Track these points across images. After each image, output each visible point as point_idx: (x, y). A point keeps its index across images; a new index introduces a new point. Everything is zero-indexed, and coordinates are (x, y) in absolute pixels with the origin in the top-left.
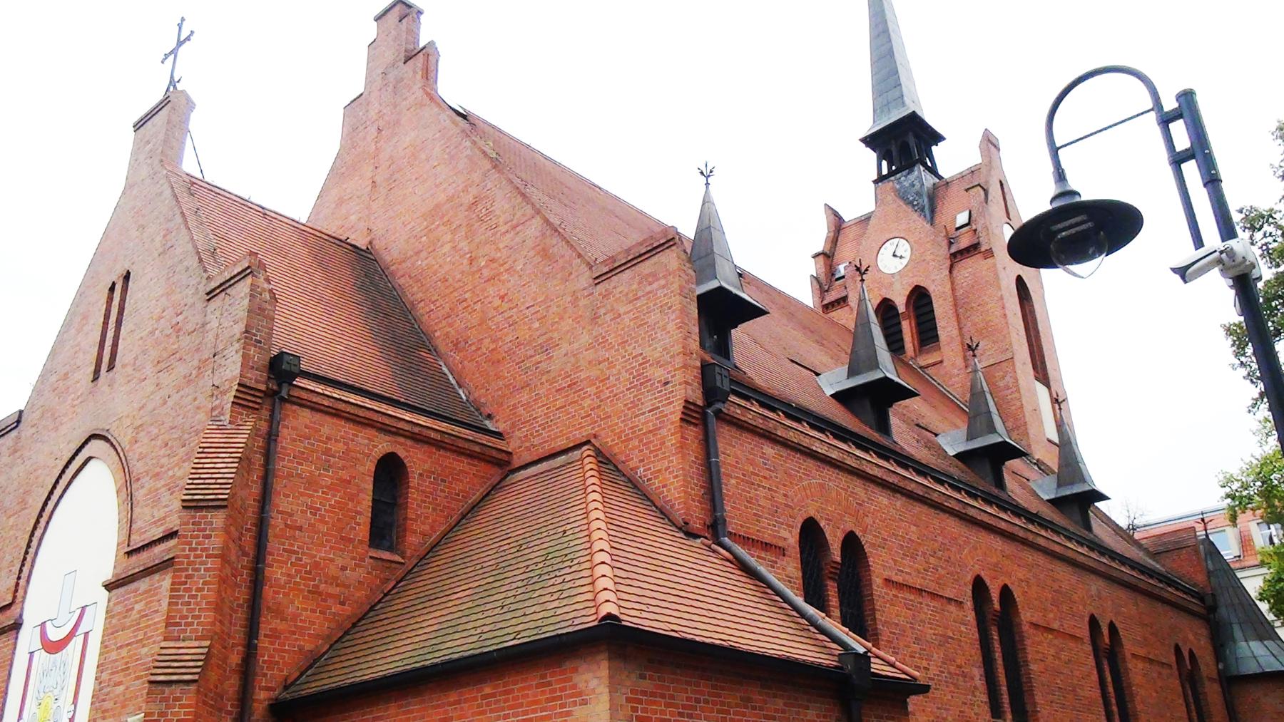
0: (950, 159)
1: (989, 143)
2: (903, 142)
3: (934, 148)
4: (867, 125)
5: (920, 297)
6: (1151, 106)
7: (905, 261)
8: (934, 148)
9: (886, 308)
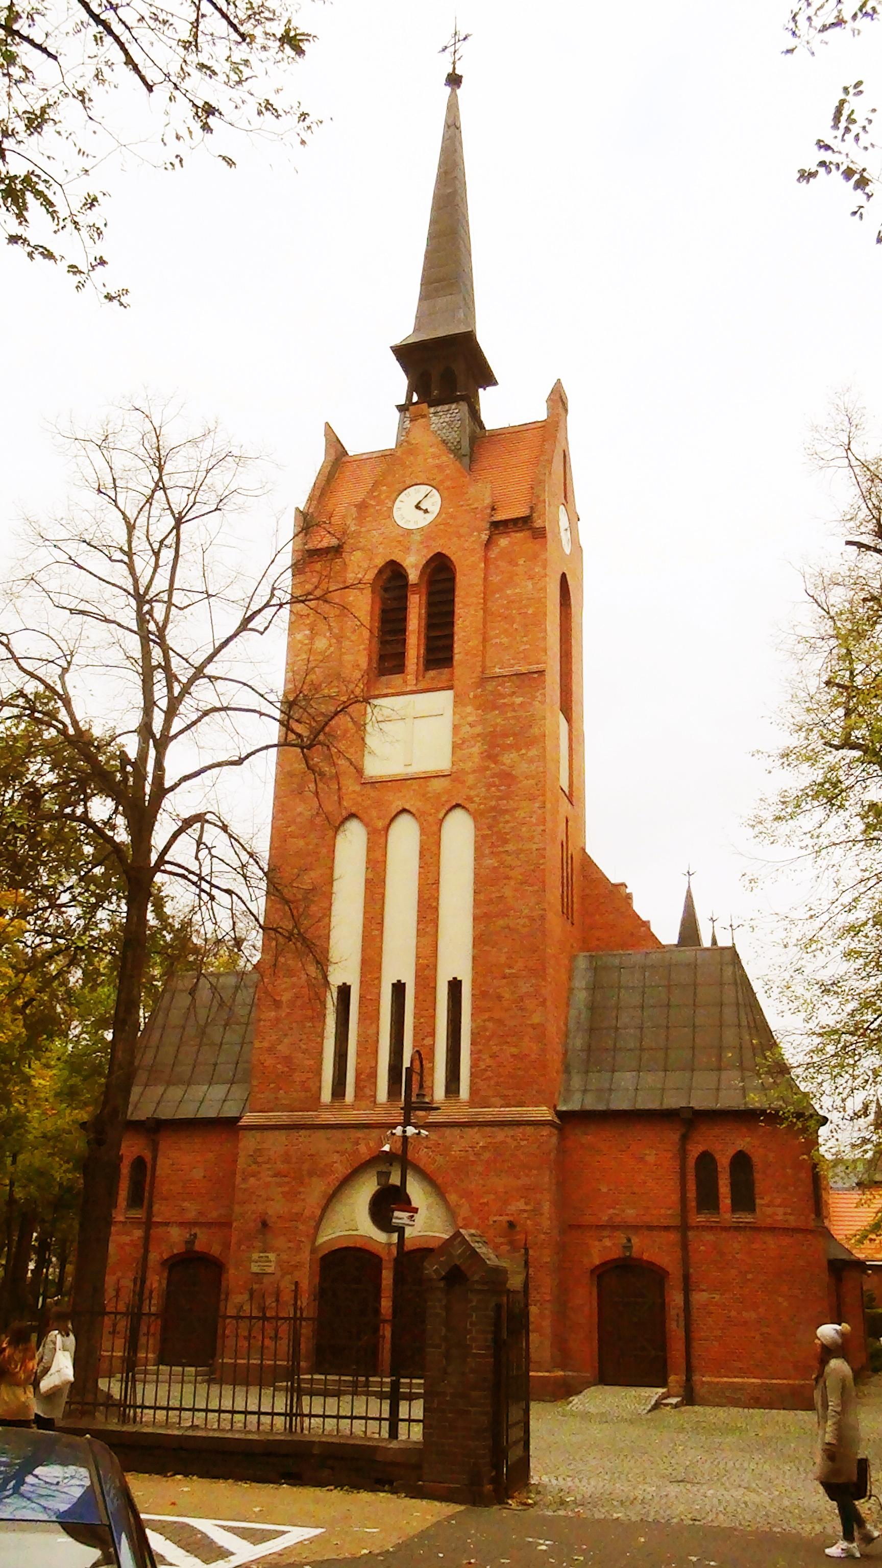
0: (498, 408)
1: (558, 400)
2: (444, 367)
3: (481, 390)
4: (404, 330)
5: (441, 570)
6: (175, 592)
7: (430, 518)
8: (481, 390)
9: (392, 577)
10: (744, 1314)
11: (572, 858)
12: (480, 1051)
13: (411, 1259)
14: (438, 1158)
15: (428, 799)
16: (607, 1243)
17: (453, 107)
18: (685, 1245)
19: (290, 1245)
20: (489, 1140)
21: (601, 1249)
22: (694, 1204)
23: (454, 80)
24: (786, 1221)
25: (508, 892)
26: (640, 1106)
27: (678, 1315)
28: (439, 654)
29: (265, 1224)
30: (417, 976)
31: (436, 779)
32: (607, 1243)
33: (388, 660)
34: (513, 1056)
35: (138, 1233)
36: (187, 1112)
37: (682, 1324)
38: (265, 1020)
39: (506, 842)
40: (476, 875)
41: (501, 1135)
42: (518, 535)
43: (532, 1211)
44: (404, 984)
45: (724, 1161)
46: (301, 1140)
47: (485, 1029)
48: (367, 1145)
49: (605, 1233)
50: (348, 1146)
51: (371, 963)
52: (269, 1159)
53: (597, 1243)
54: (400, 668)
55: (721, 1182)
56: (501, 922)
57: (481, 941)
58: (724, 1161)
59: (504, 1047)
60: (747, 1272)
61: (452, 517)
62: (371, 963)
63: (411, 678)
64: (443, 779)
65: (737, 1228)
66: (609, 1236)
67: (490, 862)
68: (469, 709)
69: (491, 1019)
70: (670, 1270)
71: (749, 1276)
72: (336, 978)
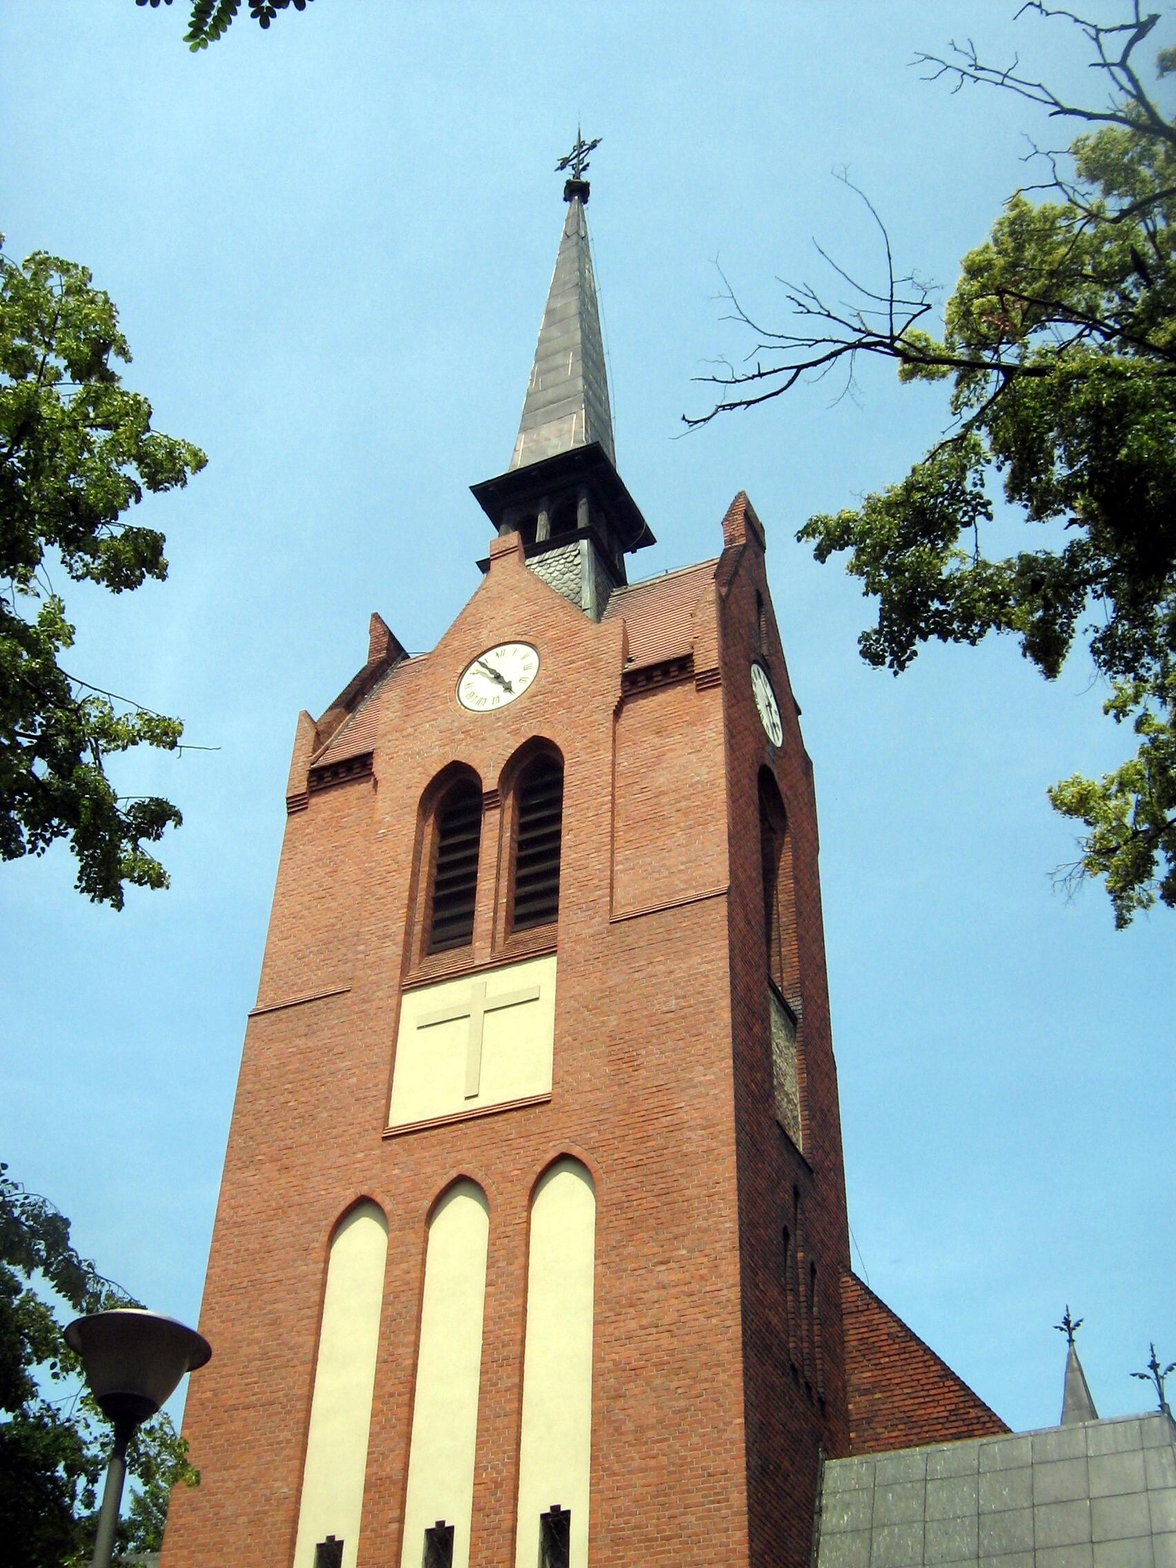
5: (538, 771)
7: (507, 698)
17: (577, 239)
23: (577, 191)
28: (535, 899)
30: (477, 1509)
33: (445, 921)
44: (452, 1528)
51: (386, 1486)
54: (466, 938)
62: (386, 1486)
63: (481, 950)
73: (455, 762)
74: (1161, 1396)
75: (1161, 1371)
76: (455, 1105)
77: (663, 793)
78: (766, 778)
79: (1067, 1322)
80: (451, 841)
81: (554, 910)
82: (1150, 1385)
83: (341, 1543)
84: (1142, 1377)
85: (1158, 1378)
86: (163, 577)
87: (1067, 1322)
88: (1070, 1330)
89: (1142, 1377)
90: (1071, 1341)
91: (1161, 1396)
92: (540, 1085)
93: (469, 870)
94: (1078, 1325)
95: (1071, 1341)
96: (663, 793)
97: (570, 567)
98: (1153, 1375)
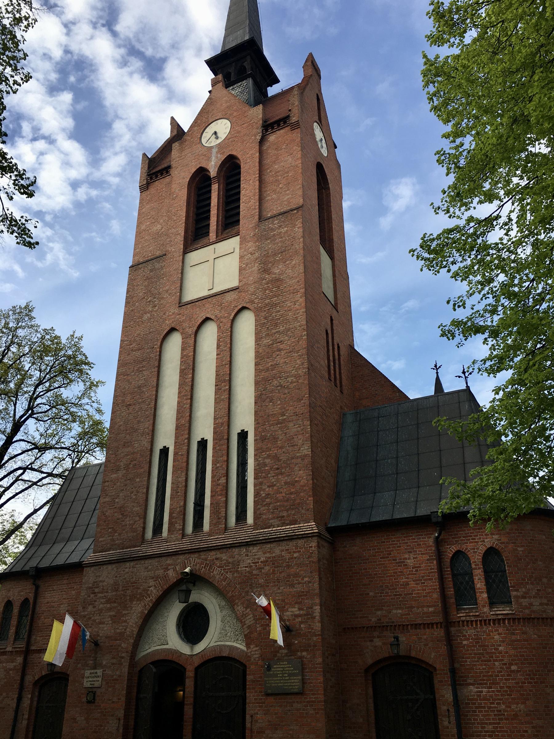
5: (231, 167)
10: (513, 707)
11: (338, 347)
12: (261, 483)
13: (223, 669)
14: (229, 575)
15: (224, 308)
16: (378, 642)
18: (449, 640)
19: (114, 661)
20: (268, 555)
21: (375, 648)
22: (453, 600)
24: (545, 611)
25: (280, 360)
26: (397, 516)
27: (448, 710)
29: (96, 644)
30: (215, 433)
31: (228, 294)
32: (378, 642)
34: (286, 483)
35: (20, 660)
36: (60, 561)
37: (453, 719)
38: (108, 481)
39: (276, 325)
40: (257, 352)
41: (277, 550)
42: (282, 131)
43: (305, 615)
45: (476, 558)
46: (127, 570)
47: (265, 465)
48: (175, 570)
49: (376, 634)
50: (160, 572)
52: (103, 589)
53: (369, 643)
54: (207, 234)
55: (476, 579)
56: (275, 382)
57: (261, 399)
58: (476, 558)
59: (280, 477)
60: (511, 664)
61: (239, 132)
63: (212, 235)
64: (232, 293)
65: (497, 621)
66: (378, 637)
67: (266, 341)
68: (250, 244)
69: (269, 456)
70: (437, 666)
71: (514, 668)
72: (159, 445)
73: (201, 167)
74: (467, 383)
75: (467, 374)
76: (205, 293)
77: (279, 172)
78: (320, 168)
79: (436, 366)
80: (201, 192)
81: (238, 221)
82: (463, 380)
83: (168, 448)
84: (459, 377)
85: (466, 377)
86: (428, 37)
87: (436, 366)
88: (437, 369)
89: (459, 377)
90: (437, 373)
91: (467, 383)
92: (235, 283)
93: (207, 208)
94: (440, 367)
95: (437, 373)
96: (279, 172)
97: (244, 88)
98: (464, 376)
